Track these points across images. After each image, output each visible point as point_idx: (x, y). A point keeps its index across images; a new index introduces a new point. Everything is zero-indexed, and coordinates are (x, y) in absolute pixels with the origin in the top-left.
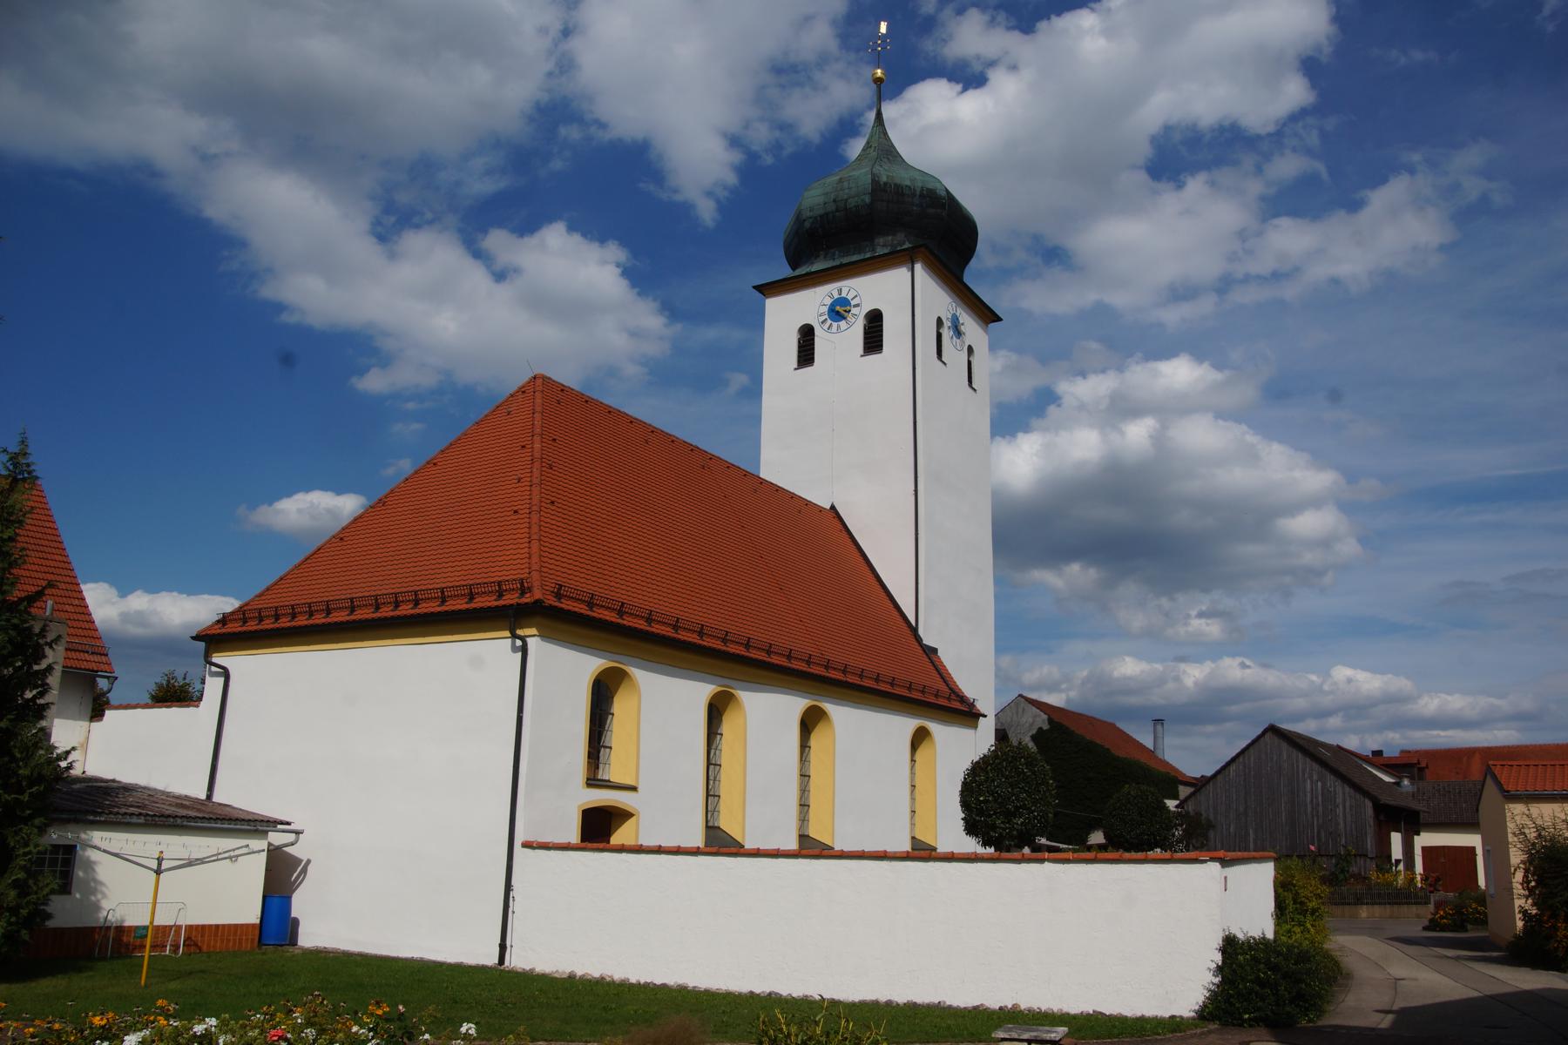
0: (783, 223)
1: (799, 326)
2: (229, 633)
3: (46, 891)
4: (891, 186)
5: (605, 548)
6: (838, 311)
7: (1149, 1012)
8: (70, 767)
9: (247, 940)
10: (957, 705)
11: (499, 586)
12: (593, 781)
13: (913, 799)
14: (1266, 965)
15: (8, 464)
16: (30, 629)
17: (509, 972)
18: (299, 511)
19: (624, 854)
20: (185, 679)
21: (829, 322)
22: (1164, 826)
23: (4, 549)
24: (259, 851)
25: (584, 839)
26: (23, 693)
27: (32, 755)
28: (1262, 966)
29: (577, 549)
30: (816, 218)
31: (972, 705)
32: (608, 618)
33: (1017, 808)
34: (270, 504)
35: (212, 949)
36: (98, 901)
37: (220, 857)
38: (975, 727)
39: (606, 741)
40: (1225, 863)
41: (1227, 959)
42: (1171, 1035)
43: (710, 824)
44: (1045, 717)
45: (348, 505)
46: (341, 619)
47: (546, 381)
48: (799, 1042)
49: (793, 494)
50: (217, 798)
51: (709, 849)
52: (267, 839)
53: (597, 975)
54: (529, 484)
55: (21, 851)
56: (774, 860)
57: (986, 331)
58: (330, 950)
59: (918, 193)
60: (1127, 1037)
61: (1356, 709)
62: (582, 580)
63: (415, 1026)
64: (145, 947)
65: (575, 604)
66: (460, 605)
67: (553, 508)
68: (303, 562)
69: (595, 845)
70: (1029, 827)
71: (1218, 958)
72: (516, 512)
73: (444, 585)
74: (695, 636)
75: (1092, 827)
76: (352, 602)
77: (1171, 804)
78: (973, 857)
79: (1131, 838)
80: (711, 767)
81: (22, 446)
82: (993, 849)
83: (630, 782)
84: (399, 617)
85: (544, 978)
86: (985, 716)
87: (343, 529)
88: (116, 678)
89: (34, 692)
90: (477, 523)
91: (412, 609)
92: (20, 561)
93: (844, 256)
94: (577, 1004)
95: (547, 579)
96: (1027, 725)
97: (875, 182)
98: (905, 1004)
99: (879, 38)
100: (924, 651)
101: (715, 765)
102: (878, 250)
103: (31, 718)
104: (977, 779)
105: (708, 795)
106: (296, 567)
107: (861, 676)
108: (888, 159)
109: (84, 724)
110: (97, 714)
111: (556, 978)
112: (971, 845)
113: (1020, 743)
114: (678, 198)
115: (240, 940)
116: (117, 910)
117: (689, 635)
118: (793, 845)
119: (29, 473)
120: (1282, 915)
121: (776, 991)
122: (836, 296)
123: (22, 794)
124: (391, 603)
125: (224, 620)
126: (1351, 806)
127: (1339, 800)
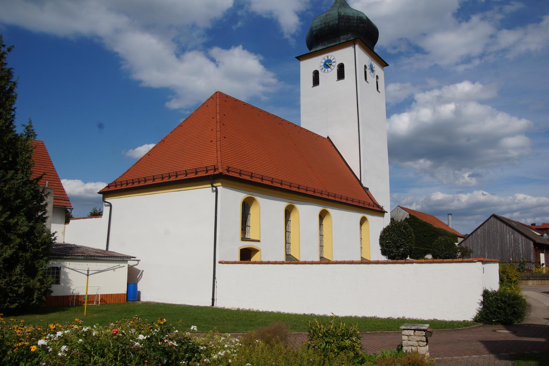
1: (315, 70)
2: (111, 191)
3: (50, 283)
5: (245, 153)
6: (327, 65)
7: (455, 319)
8: (55, 239)
9: (122, 299)
10: (377, 209)
12: (244, 239)
13: (361, 243)
14: (501, 301)
15: (26, 130)
16: (38, 190)
17: (216, 308)
19: (256, 265)
20: (100, 210)
21: (324, 69)
22: (454, 252)
23: (26, 161)
25: (241, 260)
26: (38, 213)
27: (41, 235)
28: (499, 302)
29: (234, 154)
30: (318, 30)
31: (382, 208)
32: (247, 179)
33: (401, 245)
35: (110, 303)
36: (70, 286)
38: (383, 216)
39: (248, 224)
40: (484, 262)
41: (486, 299)
42: (464, 328)
43: (287, 254)
45: (152, 146)
46: (150, 183)
49: (314, 133)
50: (110, 250)
51: (287, 262)
52: (127, 263)
53: (247, 309)
55: (40, 269)
56: (311, 265)
58: (152, 302)
59: (356, 18)
60: (447, 328)
61: (525, 210)
62: (237, 165)
63: (171, 327)
64: (85, 302)
65: (235, 174)
66: (193, 176)
67: (225, 139)
69: (245, 262)
70: (406, 252)
71: (482, 298)
72: (211, 141)
74: (279, 185)
76: (154, 177)
77: (457, 244)
79: (442, 256)
80: (287, 233)
81: (30, 124)
85: (228, 310)
86: (387, 212)
87: (150, 151)
88: (73, 209)
89: (42, 213)
92: (32, 165)
93: (329, 44)
94: (240, 319)
95: (223, 165)
96: (401, 217)
97: (339, 15)
98: (362, 317)
101: (288, 232)
103: (40, 222)
104: (385, 234)
105: (286, 243)
106: (133, 166)
108: (344, 6)
109: (63, 225)
110: (67, 222)
111: (233, 310)
112: (384, 258)
115: (120, 299)
117: (277, 184)
118: (318, 259)
119: (33, 133)
120: (502, 283)
122: (326, 59)
123: (39, 249)
124: (167, 176)
126: (525, 244)
127: (520, 241)
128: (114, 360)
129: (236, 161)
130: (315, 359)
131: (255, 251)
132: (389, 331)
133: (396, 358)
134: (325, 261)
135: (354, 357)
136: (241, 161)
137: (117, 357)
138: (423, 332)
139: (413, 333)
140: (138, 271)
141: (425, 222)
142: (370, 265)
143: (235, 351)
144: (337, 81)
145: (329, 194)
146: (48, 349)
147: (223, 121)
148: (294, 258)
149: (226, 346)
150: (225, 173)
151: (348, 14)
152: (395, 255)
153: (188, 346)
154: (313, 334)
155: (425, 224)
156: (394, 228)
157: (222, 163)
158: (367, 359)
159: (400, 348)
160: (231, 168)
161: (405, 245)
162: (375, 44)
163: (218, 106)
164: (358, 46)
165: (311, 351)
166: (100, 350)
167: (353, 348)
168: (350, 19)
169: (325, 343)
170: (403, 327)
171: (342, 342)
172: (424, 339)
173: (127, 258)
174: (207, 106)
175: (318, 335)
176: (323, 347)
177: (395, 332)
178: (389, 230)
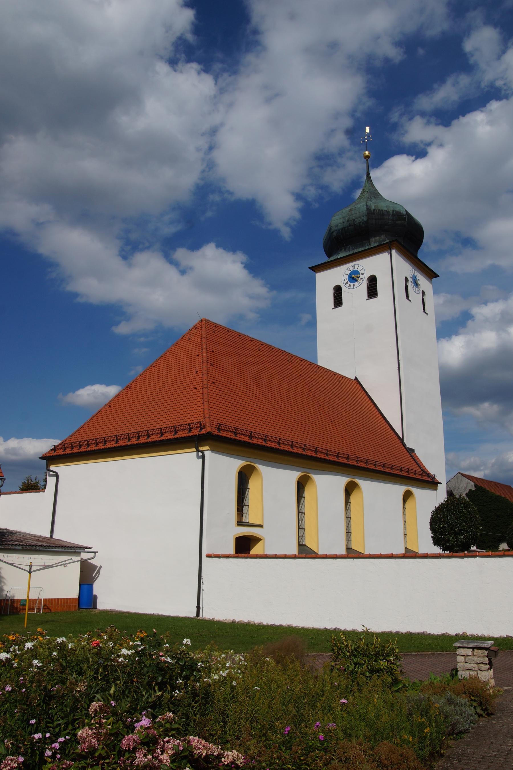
0: (321, 235)
2: (58, 455)
4: (377, 211)
6: (353, 277)
9: (73, 606)
10: (426, 478)
11: (189, 426)
12: (240, 523)
13: (405, 528)
17: (202, 620)
18: (88, 395)
20: (36, 480)
21: (349, 283)
24: (77, 561)
25: (237, 552)
29: (227, 405)
30: (339, 230)
31: (434, 478)
32: (244, 440)
33: (460, 530)
34: (74, 392)
36: (2, 586)
37: (59, 564)
38: (436, 489)
39: (246, 502)
43: (301, 543)
44: (473, 484)
45: (113, 390)
46: (112, 446)
47: (207, 322)
48: (353, 649)
49: (335, 373)
50: (55, 536)
51: (300, 556)
52: (80, 556)
53: (246, 621)
54: (201, 374)
57: (431, 283)
59: (391, 214)
63: (162, 639)
64: (25, 609)
66: (170, 436)
67: (214, 385)
68: (91, 419)
69: (243, 555)
70: (467, 540)
72: (195, 388)
73: (162, 427)
75: (501, 541)
78: (438, 555)
80: (300, 514)
82: (448, 552)
83: (259, 523)
84: (140, 444)
85: (219, 623)
86: (441, 483)
87: (110, 401)
90: (177, 395)
91: (146, 439)
95: (213, 421)
96: (463, 488)
97: (368, 209)
98: (406, 633)
99: (366, 135)
100: (407, 451)
101: (302, 513)
102: (372, 245)
105: (299, 529)
107: (375, 465)
108: (374, 197)
112: (437, 550)
113: (460, 496)
114: (271, 227)
116: (11, 591)
117: (286, 447)
118: (344, 552)
121: (338, 627)
122: (352, 270)
124: (136, 437)
125: (55, 449)
128: (93, 679)
129: (229, 416)
130: (340, 682)
131: (255, 540)
132: (443, 652)
133: (448, 685)
134: (353, 555)
135: (392, 683)
136: (236, 415)
137: (98, 675)
138: (485, 651)
139: (471, 652)
140: (93, 567)
141: (498, 496)
142: (416, 560)
143: (239, 671)
144: (367, 300)
145: (358, 458)
146: (13, 664)
147: (211, 361)
148: (310, 550)
149: (228, 665)
150: (215, 433)
151: (380, 208)
152: (452, 544)
153: (185, 662)
154: (338, 652)
155: (498, 499)
156: (450, 507)
157: (211, 419)
158: (409, 687)
159: (454, 673)
160: (223, 426)
161: (467, 530)
162: (419, 248)
163: (204, 339)
164: (396, 252)
165: (335, 672)
166: (77, 666)
167: (390, 670)
168: (383, 215)
169: (354, 664)
170: (458, 645)
171: (376, 663)
172: (486, 660)
173: (80, 549)
174: (189, 339)
175: (344, 653)
176: (350, 669)
177: (451, 653)
178: (443, 510)
